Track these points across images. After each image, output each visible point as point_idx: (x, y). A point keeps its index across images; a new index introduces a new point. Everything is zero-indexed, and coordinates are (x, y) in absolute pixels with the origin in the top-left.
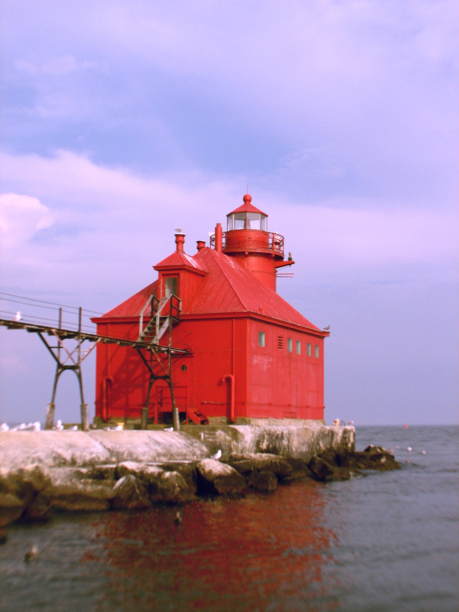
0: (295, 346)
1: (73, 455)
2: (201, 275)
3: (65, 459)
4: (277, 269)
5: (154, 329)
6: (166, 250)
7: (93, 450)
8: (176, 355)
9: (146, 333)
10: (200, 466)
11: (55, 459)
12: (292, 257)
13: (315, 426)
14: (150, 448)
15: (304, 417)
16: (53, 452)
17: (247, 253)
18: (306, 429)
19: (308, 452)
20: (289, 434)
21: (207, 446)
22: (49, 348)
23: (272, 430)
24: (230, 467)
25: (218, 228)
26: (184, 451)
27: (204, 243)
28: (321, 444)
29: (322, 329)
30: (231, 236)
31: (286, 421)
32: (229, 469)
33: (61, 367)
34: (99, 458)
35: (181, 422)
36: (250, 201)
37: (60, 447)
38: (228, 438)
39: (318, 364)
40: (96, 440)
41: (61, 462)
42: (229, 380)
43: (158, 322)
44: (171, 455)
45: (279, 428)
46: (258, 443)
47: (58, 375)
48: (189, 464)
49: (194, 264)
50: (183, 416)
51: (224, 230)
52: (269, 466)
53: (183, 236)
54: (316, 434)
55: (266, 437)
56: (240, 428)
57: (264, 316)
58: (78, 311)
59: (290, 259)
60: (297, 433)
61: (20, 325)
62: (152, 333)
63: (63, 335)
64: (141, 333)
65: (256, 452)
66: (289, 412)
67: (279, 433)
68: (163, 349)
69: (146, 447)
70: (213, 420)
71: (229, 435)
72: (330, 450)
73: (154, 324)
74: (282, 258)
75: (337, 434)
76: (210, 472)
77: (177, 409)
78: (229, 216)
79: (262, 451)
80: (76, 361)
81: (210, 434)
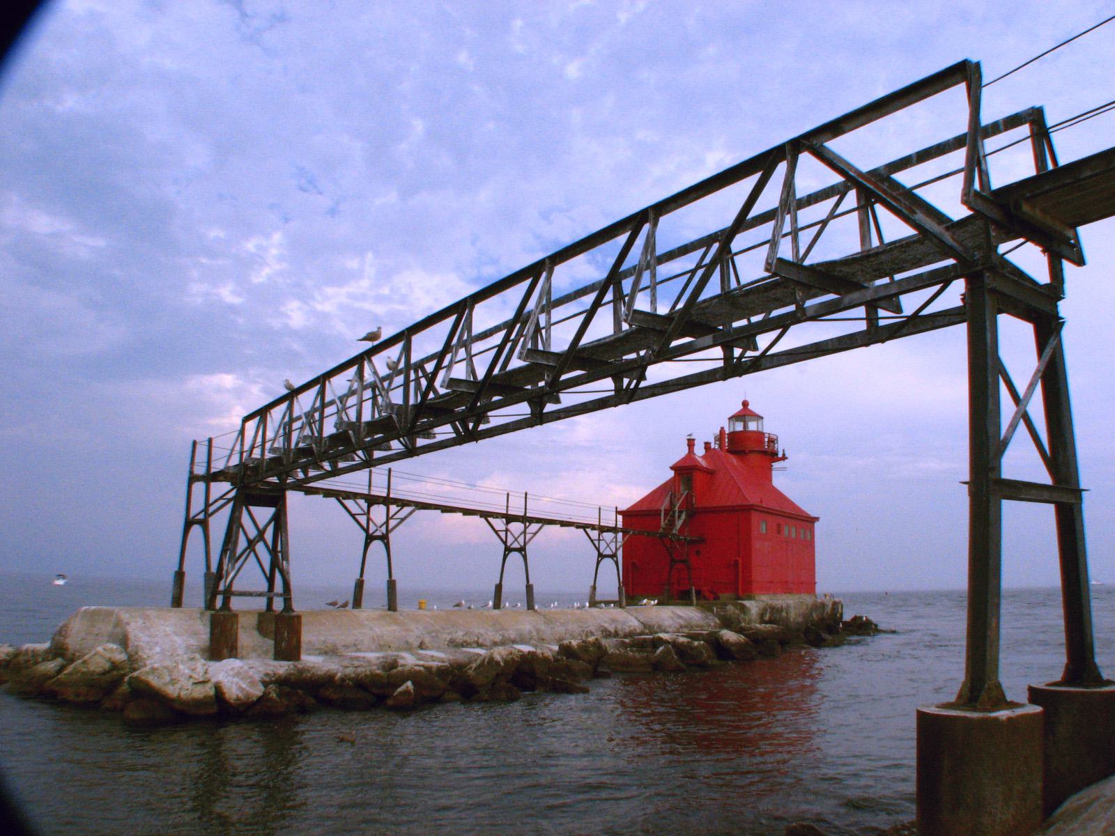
0: (790, 531)
1: (616, 628)
2: (709, 473)
3: (610, 632)
4: (773, 464)
5: (674, 521)
6: (681, 452)
7: (631, 624)
8: (692, 542)
9: (666, 525)
10: (719, 636)
11: (602, 631)
12: (786, 453)
13: (808, 599)
14: (674, 621)
15: (799, 592)
16: (601, 626)
17: (747, 451)
18: (802, 602)
19: (802, 622)
20: (788, 607)
21: (719, 619)
22: (592, 541)
23: (773, 604)
24: (743, 637)
25: (722, 429)
26: (701, 623)
27: (710, 443)
28: (814, 615)
29: (813, 514)
30: (733, 435)
31: (784, 596)
32: (742, 638)
33: (508, 550)
34: (636, 630)
35: (696, 599)
36: (748, 405)
37: (605, 622)
38: (737, 611)
39: (810, 545)
40: (632, 615)
41: (607, 634)
42: (736, 563)
43: (677, 516)
44: (692, 627)
45: (780, 602)
46: (762, 615)
47: (598, 563)
48: (707, 634)
49: (704, 463)
50: (698, 593)
51: (727, 432)
52: (771, 634)
53: (694, 440)
54: (810, 606)
55: (769, 610)
56: (747, 603)
57: (764, 508)
58: (387, 472)
59: (784, 455)
60: (793, 604)
61: (314, 490)
62: (672, 524)
63: (510, 518)
64: (663, 524)
65: (761, 623)
66: (787, 588)
67: (779, 606)
68: (681, 537)
69: (671, 620)
70: (724, 596)
71: (737, 609)
72: (822, 620)
73: (673, 516)
74: (777, 455)
75: (828, 606)
76: (728, 641)
77: (693, 588)
78: (730, 419)
79: (766, 623)
80: (522, 544)
81: (722, 608)
